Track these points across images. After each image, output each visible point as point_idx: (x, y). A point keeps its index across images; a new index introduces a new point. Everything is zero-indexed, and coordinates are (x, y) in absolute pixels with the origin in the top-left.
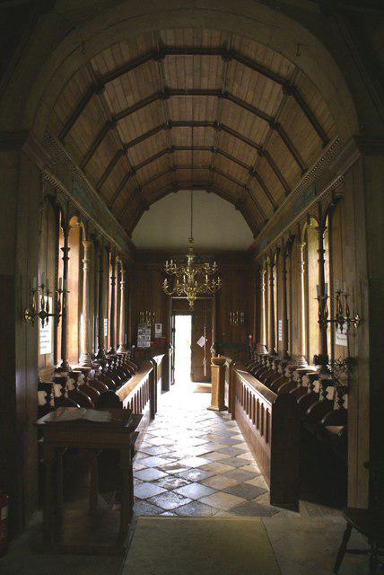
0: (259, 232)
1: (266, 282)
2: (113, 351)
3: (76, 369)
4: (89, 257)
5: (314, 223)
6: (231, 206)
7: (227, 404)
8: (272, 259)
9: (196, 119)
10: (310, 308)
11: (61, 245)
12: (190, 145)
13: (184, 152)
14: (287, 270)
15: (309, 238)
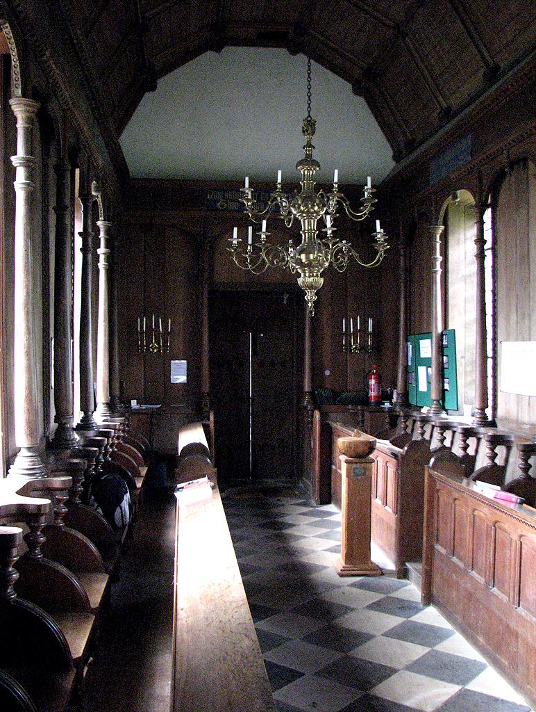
4: (30, 150)
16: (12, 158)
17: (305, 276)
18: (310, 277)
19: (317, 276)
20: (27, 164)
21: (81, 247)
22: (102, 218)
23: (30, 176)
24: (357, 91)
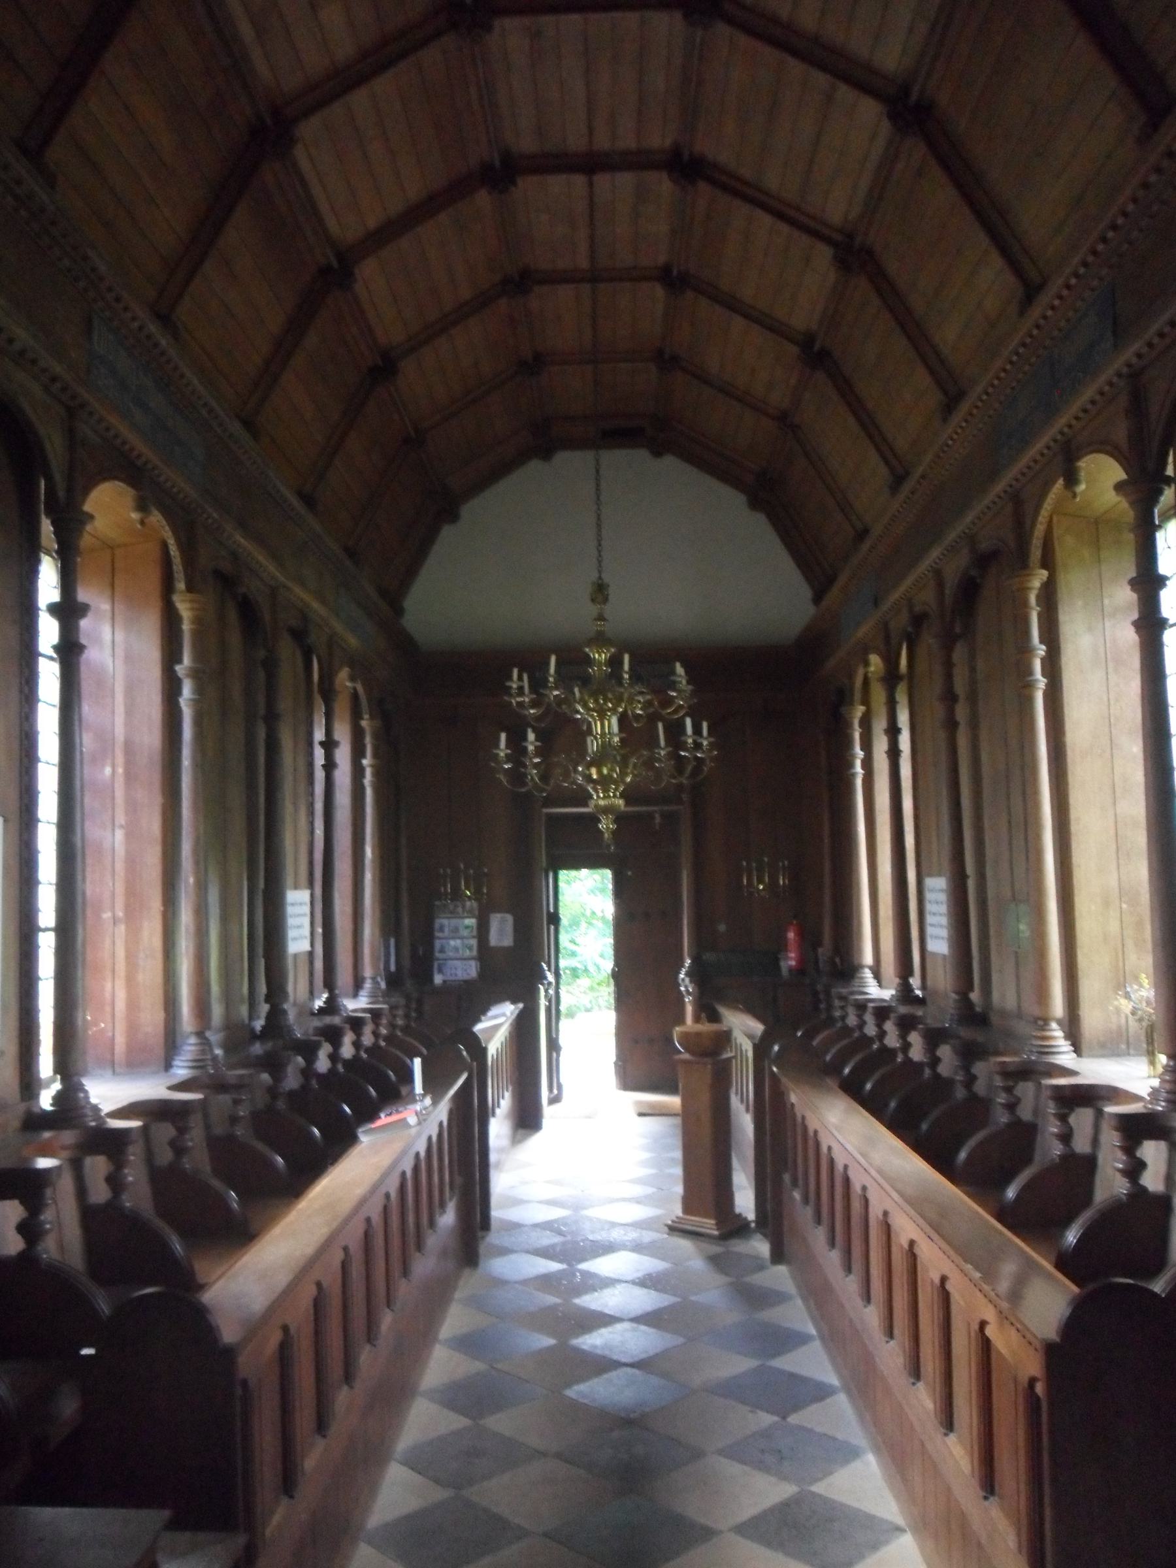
0: (831, 580)
1: (867, 746)
2: (331, 1007)
3: (355, 1011)
4: (198, 655)
5: (876, 662)
6: (733, 500)
7: (745, 1201)
8: (891, 662)
9: (602, 142)
10: (1074, 828)
11: (319, 735)
12: (584, 264)
13: (565, 293)
14: (960, 687)
15: (1059, 554)
16: (178, 668)
17: (598, 797)
18: (605, 797)
19: (615, 796)
20: (196, 674)
21: (323, 762)
22: (366, 716)
23: (199, 690)
24: (756, 503)
